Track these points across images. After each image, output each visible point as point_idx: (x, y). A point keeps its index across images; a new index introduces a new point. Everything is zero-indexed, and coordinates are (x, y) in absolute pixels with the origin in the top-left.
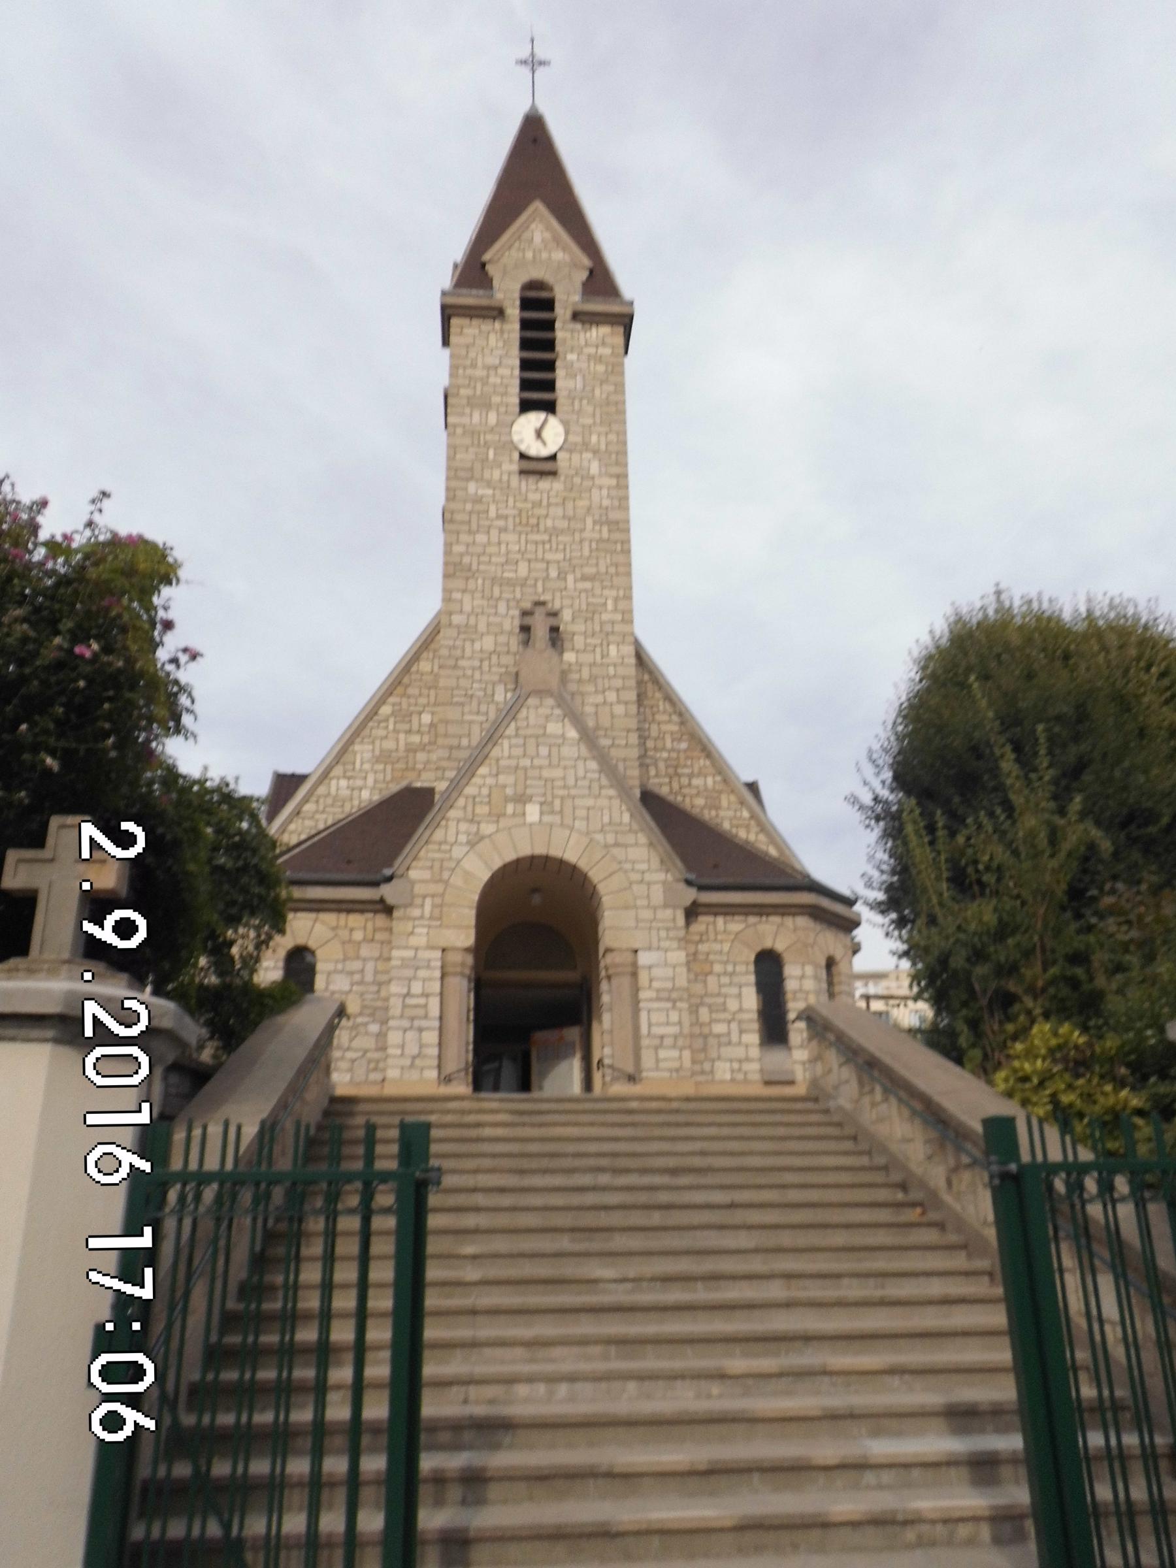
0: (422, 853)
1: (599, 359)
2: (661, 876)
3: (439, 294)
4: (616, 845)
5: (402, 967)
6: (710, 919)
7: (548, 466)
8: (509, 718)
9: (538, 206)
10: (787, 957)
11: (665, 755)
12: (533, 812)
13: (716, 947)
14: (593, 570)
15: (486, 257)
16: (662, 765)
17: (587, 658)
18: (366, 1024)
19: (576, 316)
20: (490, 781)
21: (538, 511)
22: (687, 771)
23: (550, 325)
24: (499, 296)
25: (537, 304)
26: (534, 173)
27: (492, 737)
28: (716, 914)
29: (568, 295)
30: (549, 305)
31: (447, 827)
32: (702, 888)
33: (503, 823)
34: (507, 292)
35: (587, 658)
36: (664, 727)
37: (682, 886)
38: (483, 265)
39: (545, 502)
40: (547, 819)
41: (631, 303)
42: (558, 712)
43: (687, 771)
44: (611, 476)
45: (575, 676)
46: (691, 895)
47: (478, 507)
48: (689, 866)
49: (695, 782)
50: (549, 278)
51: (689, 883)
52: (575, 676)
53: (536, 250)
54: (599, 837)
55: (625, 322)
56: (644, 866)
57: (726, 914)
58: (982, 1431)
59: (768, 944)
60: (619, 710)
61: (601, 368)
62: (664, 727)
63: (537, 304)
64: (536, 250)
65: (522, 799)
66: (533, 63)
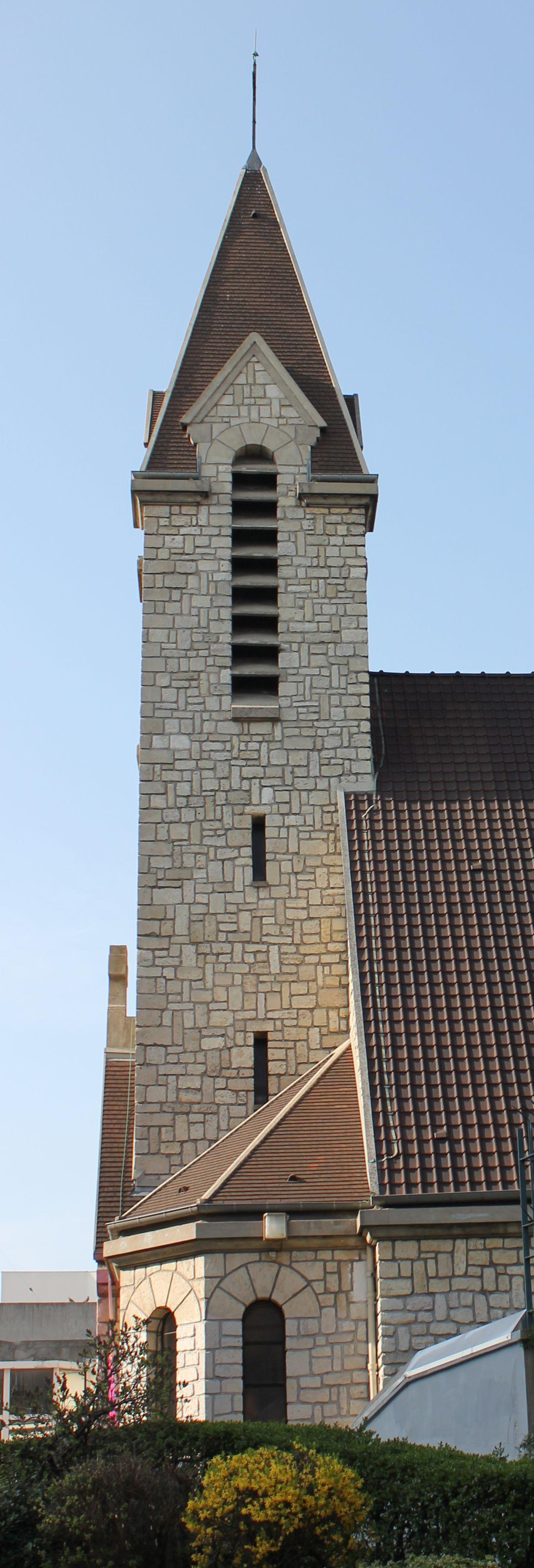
3: (130, 477)
5: (85, 1400)
9: (255, 337)
15: (186, 419)
18: (49, 1420)
19: (305, 498)
23: (269, 509)
24: (208, 471)
25: (254, 475)
26: (252, 291)
27: (213, 1049)
28: (454, 1238)
29: (292, 469)
30: (269, 481)
34: (217, 467)
38: (185, 427)
41: (373, 480)
50: (270, 445)
53: (259, 406)
55: (368, 504)
58: (249, 490)
63: (254, 475)
64: (259, 406)
66: (256, 55)
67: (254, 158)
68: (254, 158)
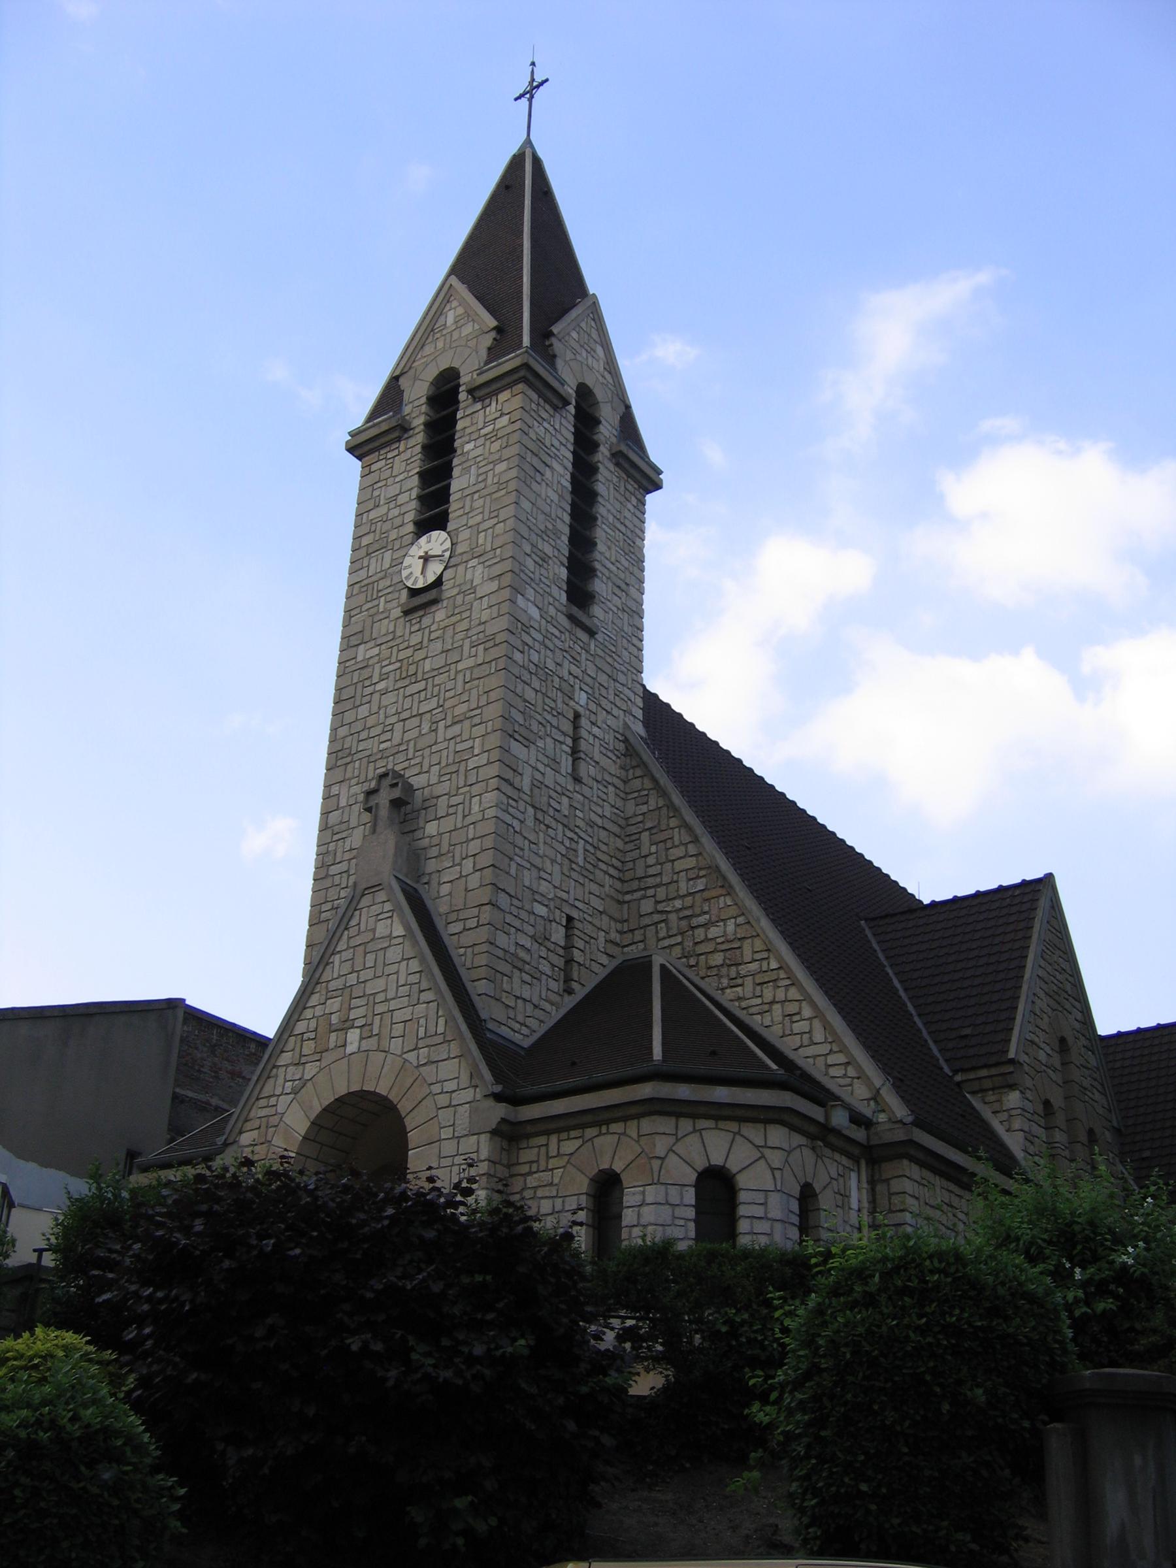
0: (252, 1115)
1: (494, 436)
2: (468, 1095)
4: (430, 1062)
6: (542, 1140)
7: (432, 594)
8: (342, 927)
10: (626, 1179)
11: (678, 904)
12: (353, 1036)
13: (545, 1177)
14: (463, 708)
16: (673, 917)
17: (447, 824)
20: (319, 1011)
21: (420, 655)
22: (702, 919)
31: (276, 1076)
32: (516, 1101)
33: (328, 1058)
35: (447, 824)
36: (679, 865)
37: (491, 1102)
39: (425, 643)
40: (365, 1045)
42: (388, 906)
43: (702, 919)
44: (491, 579)
45: (434, 852)
46: (500, 1111)
47: (366, 673)
48: (498, 1077)
49: (714, 932)
51: (498, 1098)
52: (434, 852)
54: (412, 1057)
56: (451, 1086)
57: (558, 1131)
59: (717, 1160)
60: (474, 881)
61: (496, 446)
62: (679, 865)
65: (346, 1025)
67: (528, 142)
68: (528, 142)
